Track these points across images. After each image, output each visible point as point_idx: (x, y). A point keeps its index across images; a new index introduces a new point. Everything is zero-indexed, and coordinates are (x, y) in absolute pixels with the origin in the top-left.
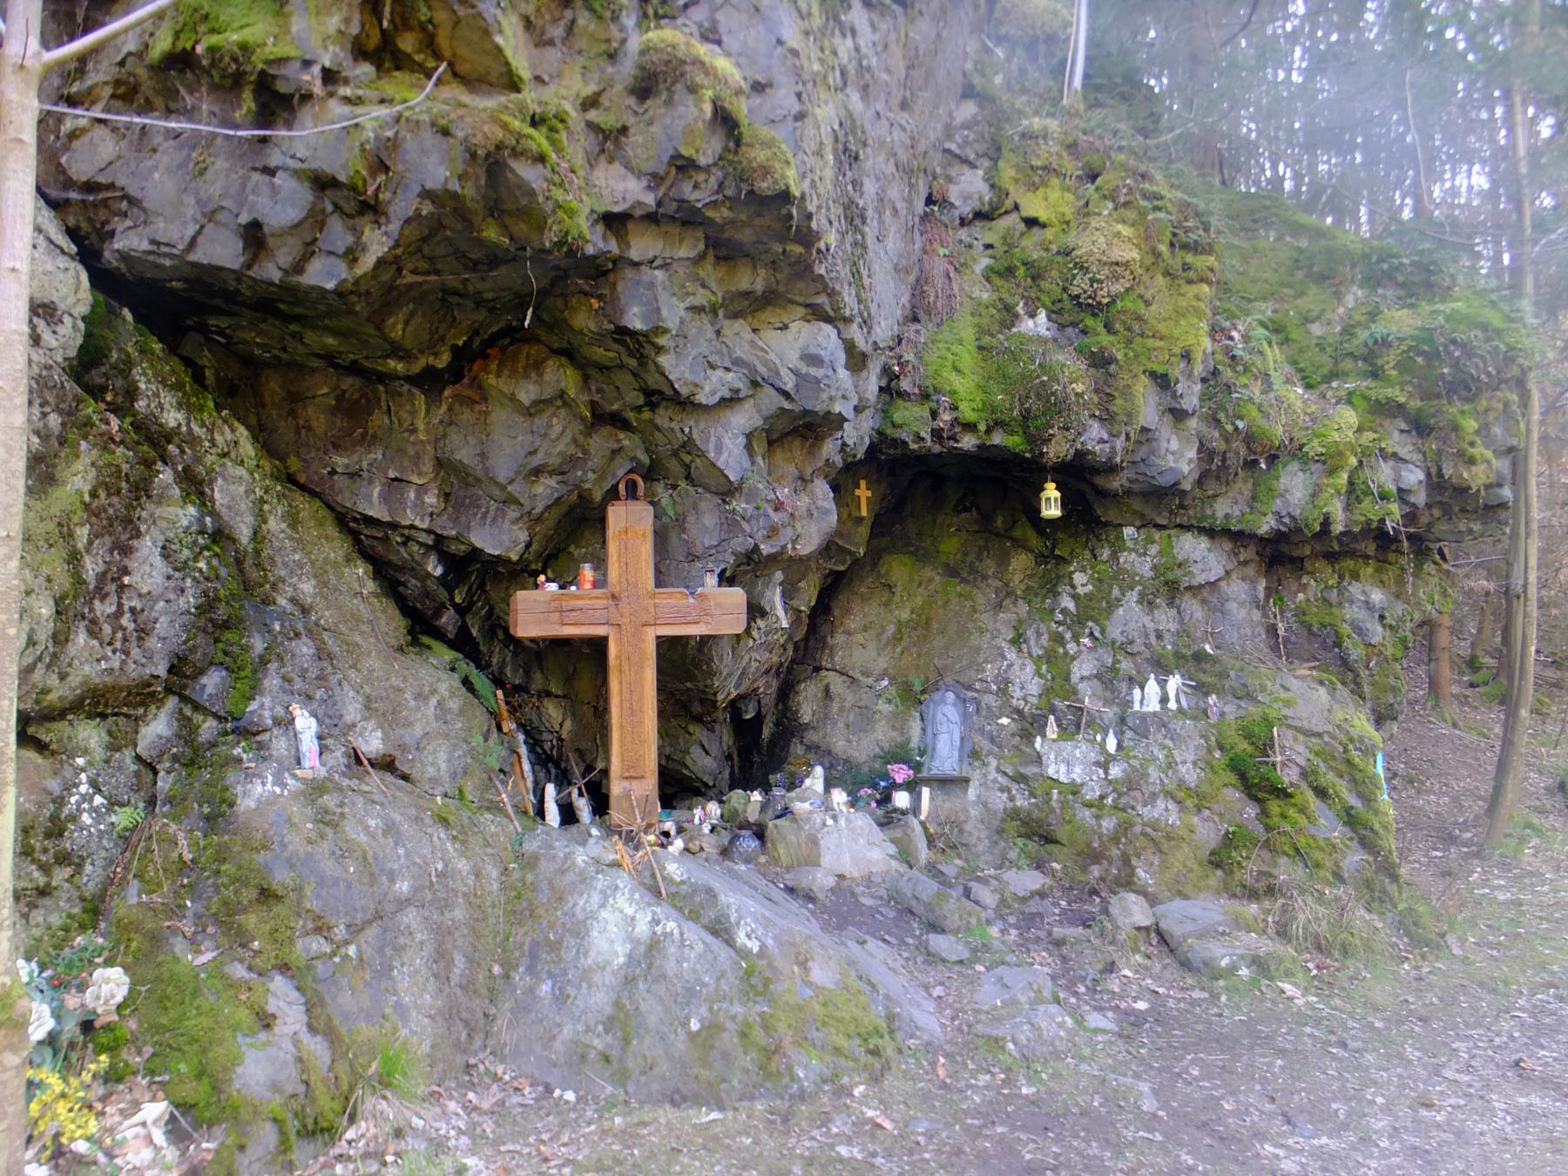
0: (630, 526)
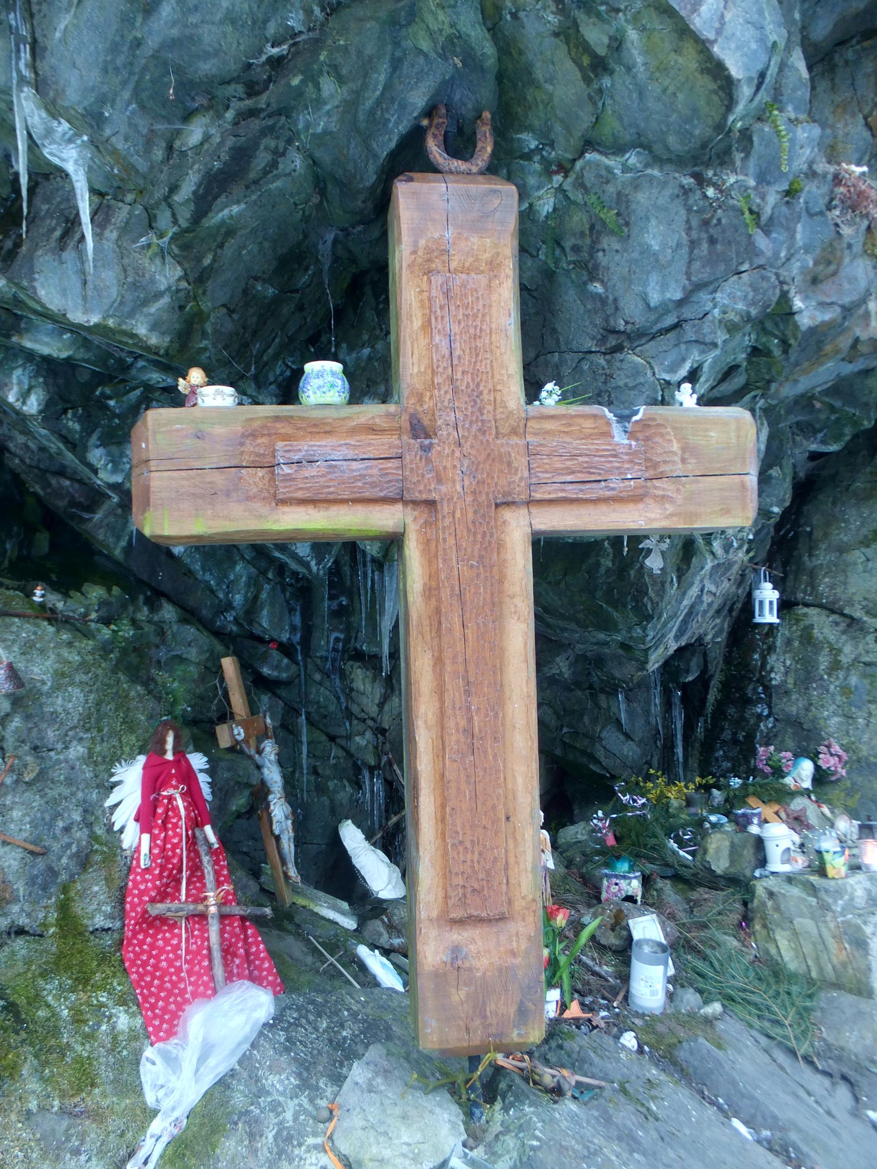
0: (453, 243)
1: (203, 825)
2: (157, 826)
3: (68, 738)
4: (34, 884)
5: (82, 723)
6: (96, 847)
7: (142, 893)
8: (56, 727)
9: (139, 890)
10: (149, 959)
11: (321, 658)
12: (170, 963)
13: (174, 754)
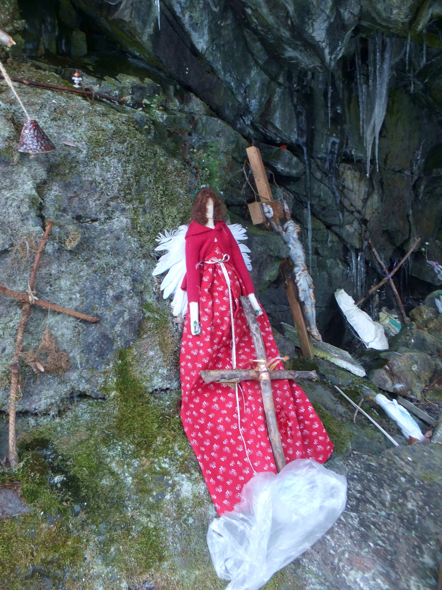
1: (248, 294)
2: (204, 294)
3: (109, 209)
4: (90, 351)
5: (122, 193)
6: (148, 314)
7: (195, 359)
8: (97, 196)
9: (192, 355)
10: (206, 422)
11: (321, 159)
12: (227, 426)
13: (215, 223)
